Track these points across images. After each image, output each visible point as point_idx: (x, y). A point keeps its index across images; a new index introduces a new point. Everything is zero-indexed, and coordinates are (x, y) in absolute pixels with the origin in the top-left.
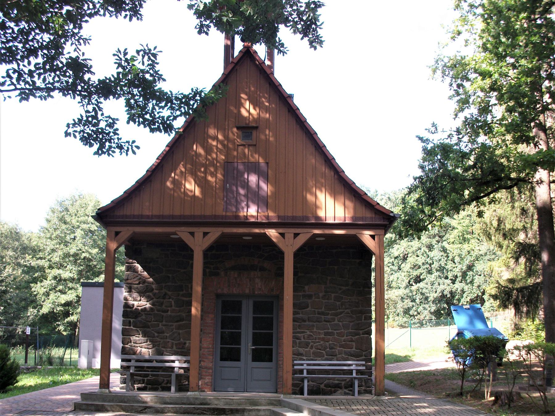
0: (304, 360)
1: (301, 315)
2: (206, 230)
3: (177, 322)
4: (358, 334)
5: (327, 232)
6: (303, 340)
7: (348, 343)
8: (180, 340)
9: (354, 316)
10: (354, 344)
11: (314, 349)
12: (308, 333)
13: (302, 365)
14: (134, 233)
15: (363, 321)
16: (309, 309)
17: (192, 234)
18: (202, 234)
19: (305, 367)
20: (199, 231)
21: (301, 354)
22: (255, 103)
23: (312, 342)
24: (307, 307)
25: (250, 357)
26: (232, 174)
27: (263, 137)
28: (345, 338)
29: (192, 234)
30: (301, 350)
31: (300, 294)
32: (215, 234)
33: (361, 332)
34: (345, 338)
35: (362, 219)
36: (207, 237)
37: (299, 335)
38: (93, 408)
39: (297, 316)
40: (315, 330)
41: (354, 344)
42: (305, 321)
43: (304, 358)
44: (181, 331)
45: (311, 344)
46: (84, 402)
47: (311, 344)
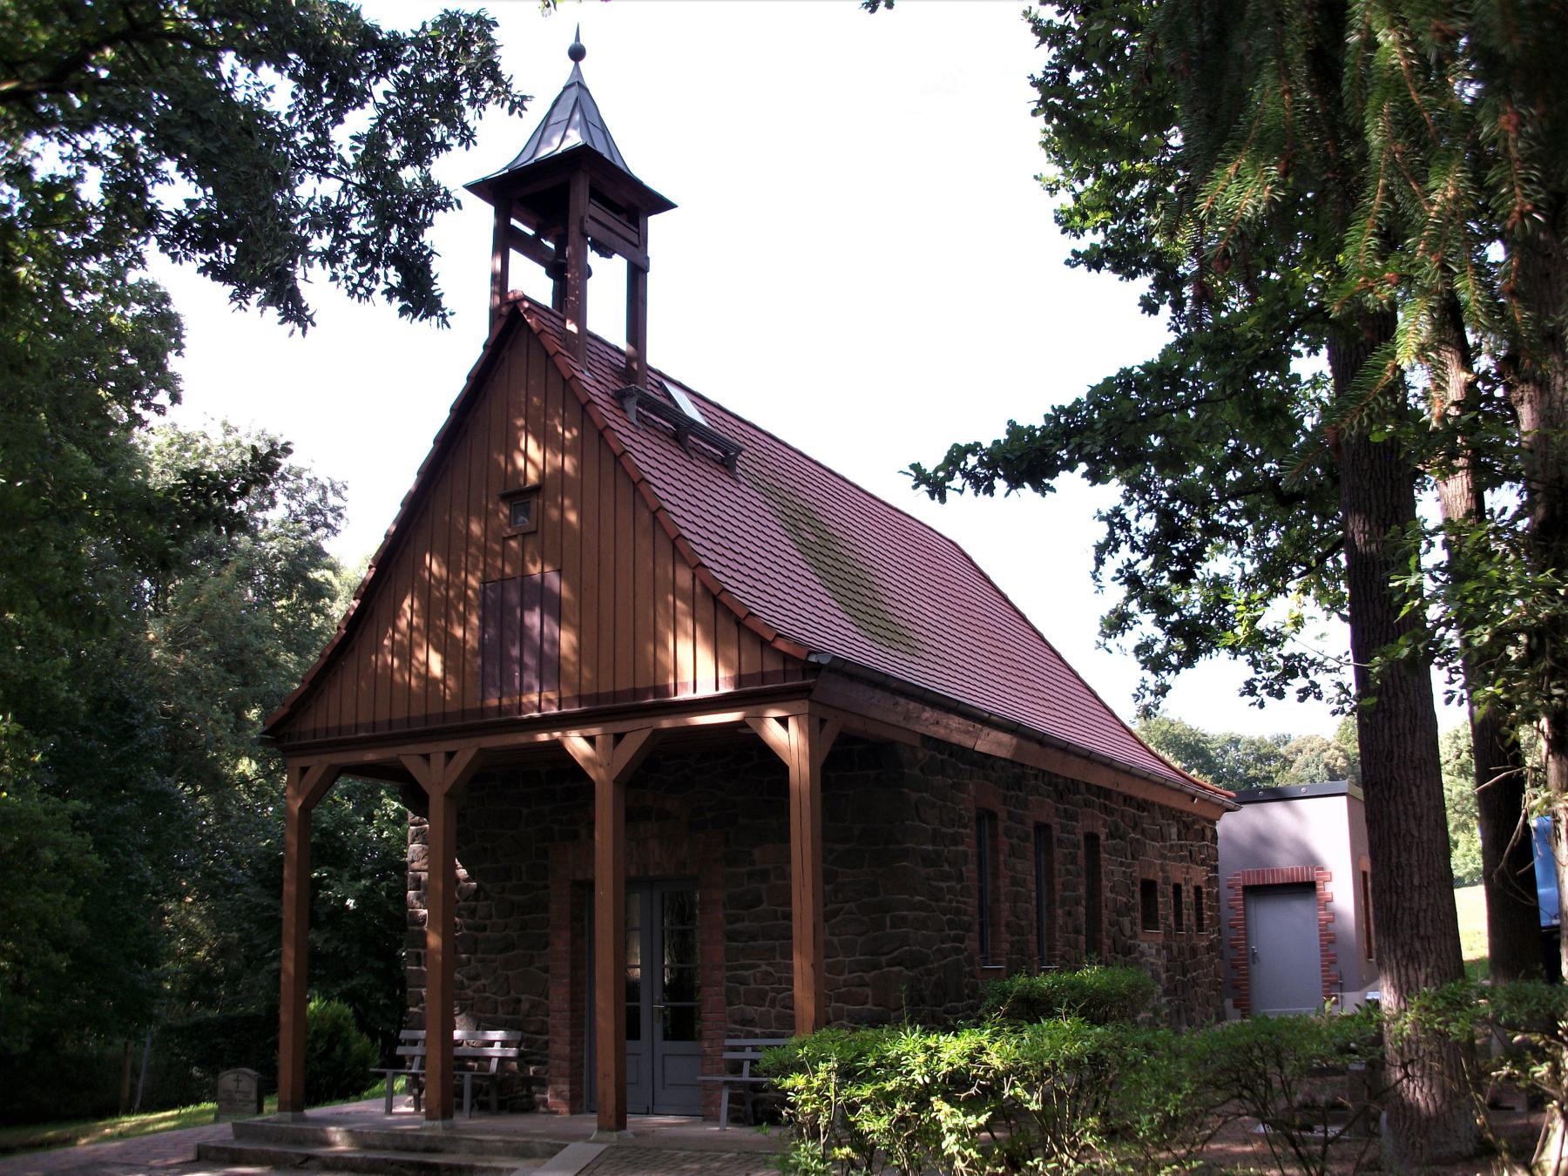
0: (756, 1036)
1: (746, 923)
2: (449, 746)
3: (501, 951)
4: (876, 966)
5: (522, 739)
6: (753, 986)
7: (854, 989)
8: (508, 993)
9: (866, 919)
10: (869, 991)
11: (778, 1008)
12: (764, 968)
13: (742, 1049)
14: (481, 751)
15: (888, 930)
16: (764, 906)
17: (426, 757)
18: (442, 756)
19: (748, 1054)
20: (437, 750)
21: (752, 1022)
22: (546, 439)
23: (773, 990)
24: (759, 902)
25: (659, 1028)
26: (502, 606)
27: (554, 514)
28: (846, 976)
29: (426, 757)
30: (752, 1011)
31: (744, 870)
32: (466, 751)
33: (884, 959)
34: (846, 976)
35: (763, 677)
36: (307, 776)
37: (745, 973)
38: (226, 1156)
39: (738, 926)
40: (778, 959)
41: (869, 991)
42: (754, 938)
43: (758, 1031)
44: (510, 973)
45: (771, 995)
46: (236, 1146)
47: (771, 995)
